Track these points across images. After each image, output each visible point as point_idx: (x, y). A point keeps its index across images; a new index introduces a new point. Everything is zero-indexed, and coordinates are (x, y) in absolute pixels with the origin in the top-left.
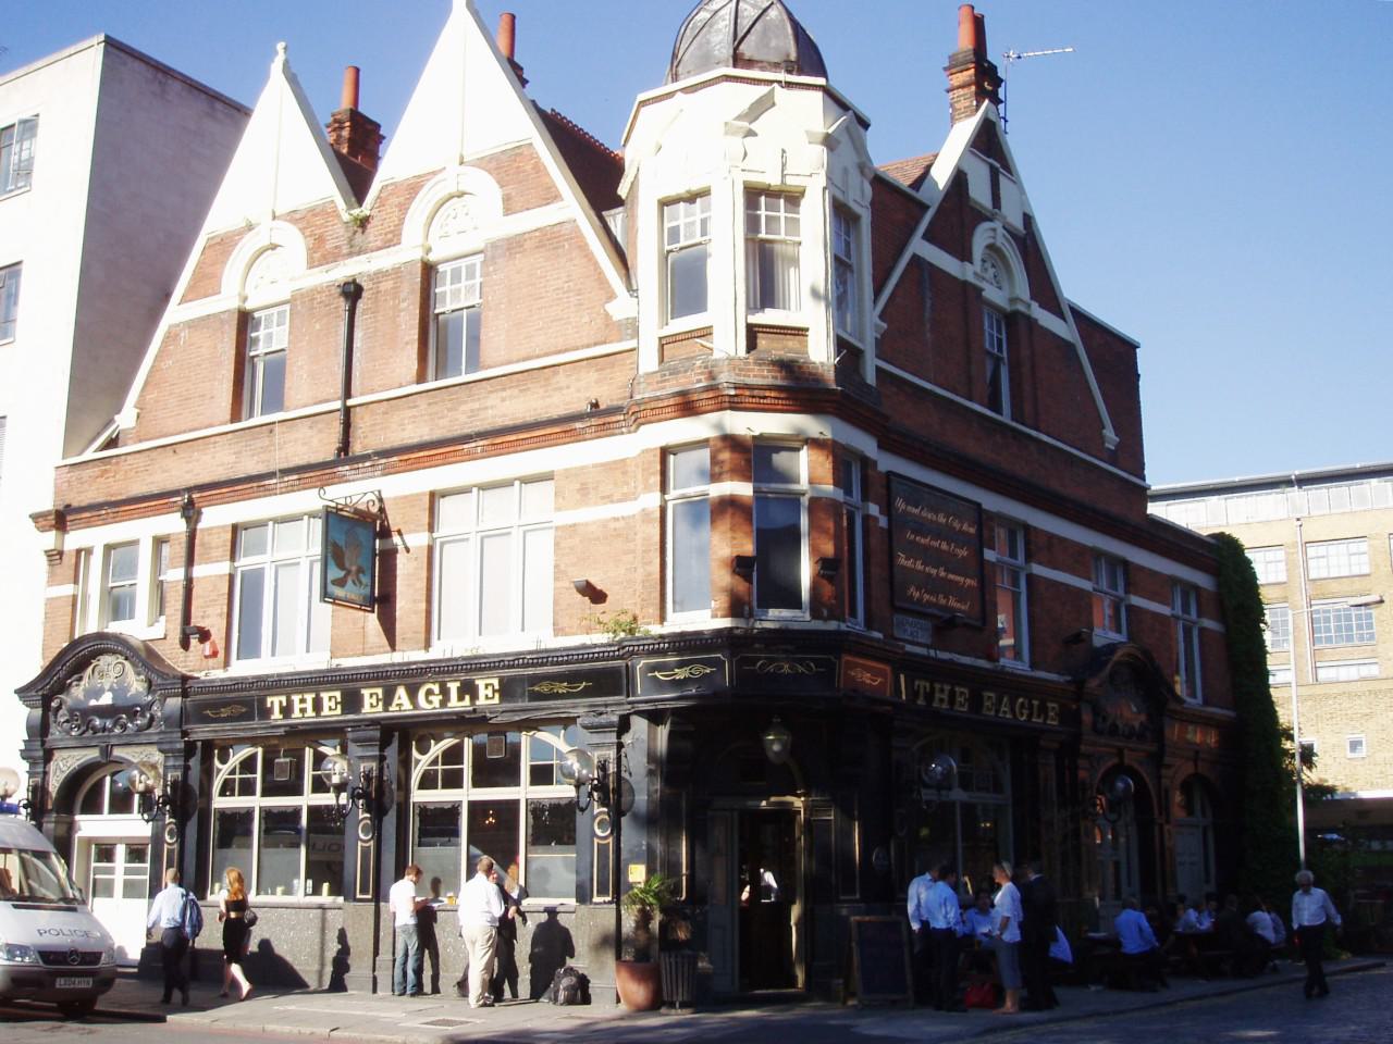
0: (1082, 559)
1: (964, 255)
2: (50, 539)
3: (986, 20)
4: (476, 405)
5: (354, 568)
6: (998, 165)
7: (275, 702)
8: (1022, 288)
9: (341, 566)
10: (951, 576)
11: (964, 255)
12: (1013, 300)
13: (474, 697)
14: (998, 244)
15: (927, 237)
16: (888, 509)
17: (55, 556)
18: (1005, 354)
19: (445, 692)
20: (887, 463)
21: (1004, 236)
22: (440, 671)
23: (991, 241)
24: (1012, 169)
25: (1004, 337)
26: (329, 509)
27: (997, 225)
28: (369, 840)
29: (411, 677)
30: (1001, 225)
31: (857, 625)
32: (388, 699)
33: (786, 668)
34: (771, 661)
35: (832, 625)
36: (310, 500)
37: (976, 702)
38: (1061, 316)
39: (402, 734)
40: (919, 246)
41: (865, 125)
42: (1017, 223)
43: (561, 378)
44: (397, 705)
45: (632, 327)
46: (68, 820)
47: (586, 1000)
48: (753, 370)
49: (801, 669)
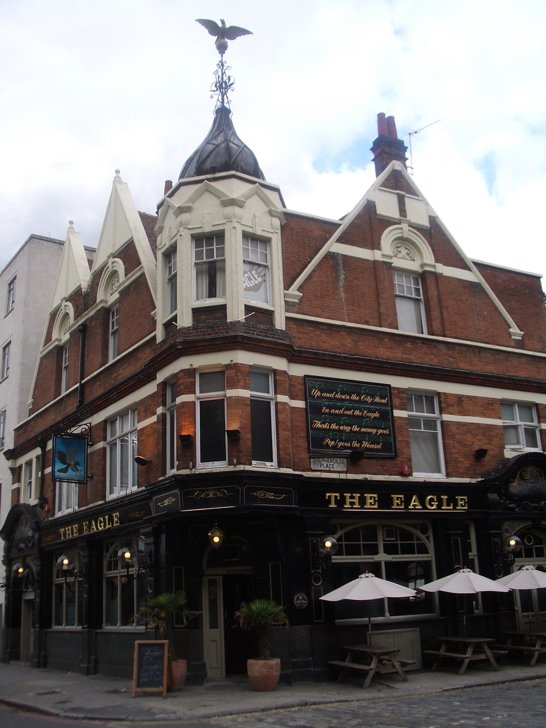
0: (489, 407)
1: (375, 245)
3: (395, 120)
5: (72, 463)
6: (403, 193)
8: (428, 257)
9: (63, 462)
10: (363, 430)
12: (423, 265)
13: (113, 523)
14: (406, 236)
17: (13, 470)
18: (422, 297)
20: (299, 370)
21: (409, 230)
23: (400, 235)
24: (418, 193)
25: (420, 287)
28: (314, 573)
30: (407, 225)
33: (211, 495)
34: (203, 491)
35: (241, 467)
42: (426, 223)
43: (140, 355)
44: (413, 505)
48: (192, 333)
49: (219, 495)
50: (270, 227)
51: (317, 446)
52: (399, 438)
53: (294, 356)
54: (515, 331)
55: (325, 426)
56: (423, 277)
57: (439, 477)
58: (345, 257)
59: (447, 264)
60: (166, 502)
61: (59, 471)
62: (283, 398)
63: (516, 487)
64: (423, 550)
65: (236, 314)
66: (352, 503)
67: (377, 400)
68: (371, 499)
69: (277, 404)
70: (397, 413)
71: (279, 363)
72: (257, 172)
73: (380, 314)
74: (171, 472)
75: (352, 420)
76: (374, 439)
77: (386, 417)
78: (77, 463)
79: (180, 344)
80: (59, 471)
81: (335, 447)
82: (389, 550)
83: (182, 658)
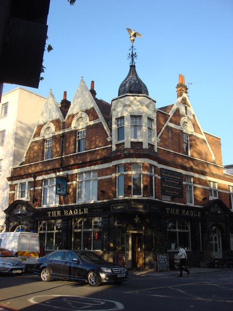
2: (9, 183)
4: (84, 157)
7: (49, 213)
11: (179, 125)
16: (161, 175)
19: (78, 211)
20: (160, 166)
22: (78, 207)
26: (91, 118)
29: (73, 208)
31: (153, 198)
32: (69, 212)
36: (53, 175)
37: (180, 212)
39: (70, 218)
41: (155, 102)
45: (111, 142)
46: (17, 136)
47: (182, 277)
50: (154, 116)
51: (164, 192)
52: (184, 191)
53: (160, 161)
55: (166, 185)
57: (192, 205)
60: (119, 207)
62: (157, 175)
63: (212, 210)
64: (187, 229)
66: (172, 211)
67: (178, 178)
68: (177, 211)
69: (155, 177)
70: (184, 183)
72: (147, 92)
73: (180, 149)
74: (121, 197)
75: (173, 184)
76: (177, 191)
77: (181, 184)
78: (64, 188)
79: (121, 152)
81: (168, 193)
82: (179, 228)
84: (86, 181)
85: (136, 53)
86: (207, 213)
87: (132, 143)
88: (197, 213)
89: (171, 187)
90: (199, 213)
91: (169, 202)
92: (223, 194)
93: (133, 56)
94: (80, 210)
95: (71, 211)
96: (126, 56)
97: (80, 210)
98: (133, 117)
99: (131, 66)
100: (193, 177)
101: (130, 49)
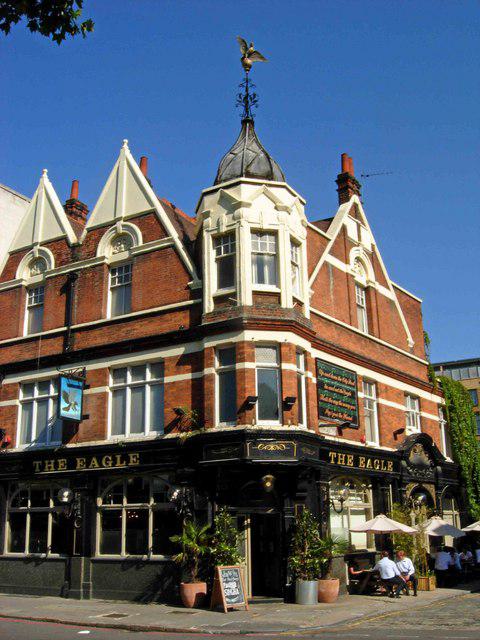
1: (347, 261)
4: (129, 328)
8: (372, 276)
9: (67, 401)
11: (347, 261)
13: (128, 461)
15: (332, 252)
19: (114, 460)
20: (315, 353)
27: (360, 248)
31: (303, 427)
32: (88, 464)
33: (272, 448)
37: (72, 464)
38: (388, 288)
40: (327, 257)
53: (318, 344)
54: (410, 339)
56: (367, 290)
58: (333, 267)
59: (381, 284)
61: (64, 409)
65: (287, 303)
67: (350, 382)
68: (62, 462)
71: (306, 345)
77: (354, 396)
78: (76, 404)
80: (64, 409)
83: (203, 580)
84: (134, 388)
85: (254, 95)
86: (404, 463)
87: (256, 293)
88: (386, 465)
89: (337, 403)
90: (390, 465)
91: (333, 439)
92: (430, 422)
93: (247, 100)
94: (118, 457)
95: (94, 459)
96: (234, 99)
97: (118, 457)
98: (258, 232)
99: (244, 122)
100: (376, 382)
101: (242, 85)
